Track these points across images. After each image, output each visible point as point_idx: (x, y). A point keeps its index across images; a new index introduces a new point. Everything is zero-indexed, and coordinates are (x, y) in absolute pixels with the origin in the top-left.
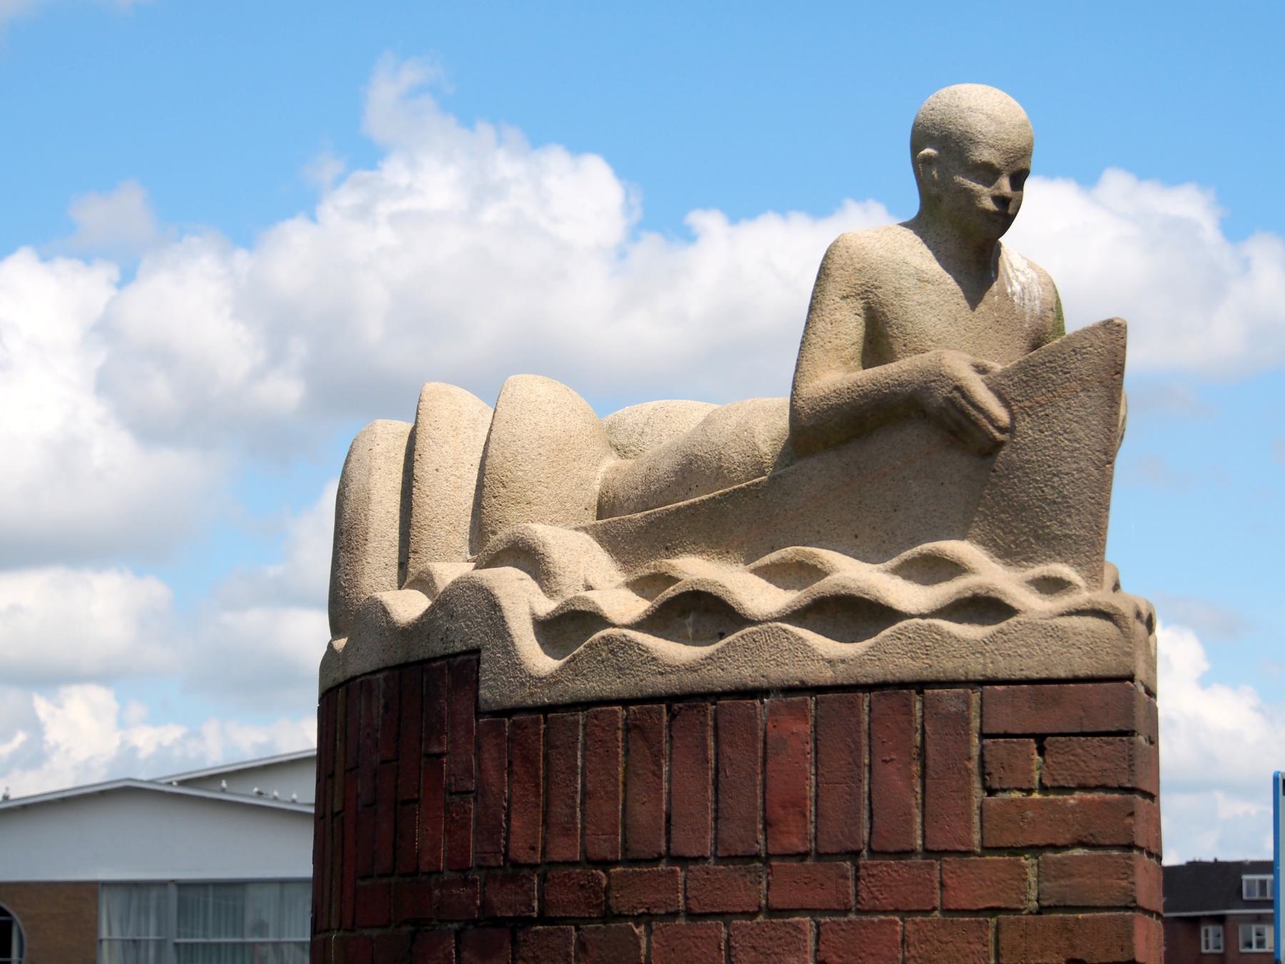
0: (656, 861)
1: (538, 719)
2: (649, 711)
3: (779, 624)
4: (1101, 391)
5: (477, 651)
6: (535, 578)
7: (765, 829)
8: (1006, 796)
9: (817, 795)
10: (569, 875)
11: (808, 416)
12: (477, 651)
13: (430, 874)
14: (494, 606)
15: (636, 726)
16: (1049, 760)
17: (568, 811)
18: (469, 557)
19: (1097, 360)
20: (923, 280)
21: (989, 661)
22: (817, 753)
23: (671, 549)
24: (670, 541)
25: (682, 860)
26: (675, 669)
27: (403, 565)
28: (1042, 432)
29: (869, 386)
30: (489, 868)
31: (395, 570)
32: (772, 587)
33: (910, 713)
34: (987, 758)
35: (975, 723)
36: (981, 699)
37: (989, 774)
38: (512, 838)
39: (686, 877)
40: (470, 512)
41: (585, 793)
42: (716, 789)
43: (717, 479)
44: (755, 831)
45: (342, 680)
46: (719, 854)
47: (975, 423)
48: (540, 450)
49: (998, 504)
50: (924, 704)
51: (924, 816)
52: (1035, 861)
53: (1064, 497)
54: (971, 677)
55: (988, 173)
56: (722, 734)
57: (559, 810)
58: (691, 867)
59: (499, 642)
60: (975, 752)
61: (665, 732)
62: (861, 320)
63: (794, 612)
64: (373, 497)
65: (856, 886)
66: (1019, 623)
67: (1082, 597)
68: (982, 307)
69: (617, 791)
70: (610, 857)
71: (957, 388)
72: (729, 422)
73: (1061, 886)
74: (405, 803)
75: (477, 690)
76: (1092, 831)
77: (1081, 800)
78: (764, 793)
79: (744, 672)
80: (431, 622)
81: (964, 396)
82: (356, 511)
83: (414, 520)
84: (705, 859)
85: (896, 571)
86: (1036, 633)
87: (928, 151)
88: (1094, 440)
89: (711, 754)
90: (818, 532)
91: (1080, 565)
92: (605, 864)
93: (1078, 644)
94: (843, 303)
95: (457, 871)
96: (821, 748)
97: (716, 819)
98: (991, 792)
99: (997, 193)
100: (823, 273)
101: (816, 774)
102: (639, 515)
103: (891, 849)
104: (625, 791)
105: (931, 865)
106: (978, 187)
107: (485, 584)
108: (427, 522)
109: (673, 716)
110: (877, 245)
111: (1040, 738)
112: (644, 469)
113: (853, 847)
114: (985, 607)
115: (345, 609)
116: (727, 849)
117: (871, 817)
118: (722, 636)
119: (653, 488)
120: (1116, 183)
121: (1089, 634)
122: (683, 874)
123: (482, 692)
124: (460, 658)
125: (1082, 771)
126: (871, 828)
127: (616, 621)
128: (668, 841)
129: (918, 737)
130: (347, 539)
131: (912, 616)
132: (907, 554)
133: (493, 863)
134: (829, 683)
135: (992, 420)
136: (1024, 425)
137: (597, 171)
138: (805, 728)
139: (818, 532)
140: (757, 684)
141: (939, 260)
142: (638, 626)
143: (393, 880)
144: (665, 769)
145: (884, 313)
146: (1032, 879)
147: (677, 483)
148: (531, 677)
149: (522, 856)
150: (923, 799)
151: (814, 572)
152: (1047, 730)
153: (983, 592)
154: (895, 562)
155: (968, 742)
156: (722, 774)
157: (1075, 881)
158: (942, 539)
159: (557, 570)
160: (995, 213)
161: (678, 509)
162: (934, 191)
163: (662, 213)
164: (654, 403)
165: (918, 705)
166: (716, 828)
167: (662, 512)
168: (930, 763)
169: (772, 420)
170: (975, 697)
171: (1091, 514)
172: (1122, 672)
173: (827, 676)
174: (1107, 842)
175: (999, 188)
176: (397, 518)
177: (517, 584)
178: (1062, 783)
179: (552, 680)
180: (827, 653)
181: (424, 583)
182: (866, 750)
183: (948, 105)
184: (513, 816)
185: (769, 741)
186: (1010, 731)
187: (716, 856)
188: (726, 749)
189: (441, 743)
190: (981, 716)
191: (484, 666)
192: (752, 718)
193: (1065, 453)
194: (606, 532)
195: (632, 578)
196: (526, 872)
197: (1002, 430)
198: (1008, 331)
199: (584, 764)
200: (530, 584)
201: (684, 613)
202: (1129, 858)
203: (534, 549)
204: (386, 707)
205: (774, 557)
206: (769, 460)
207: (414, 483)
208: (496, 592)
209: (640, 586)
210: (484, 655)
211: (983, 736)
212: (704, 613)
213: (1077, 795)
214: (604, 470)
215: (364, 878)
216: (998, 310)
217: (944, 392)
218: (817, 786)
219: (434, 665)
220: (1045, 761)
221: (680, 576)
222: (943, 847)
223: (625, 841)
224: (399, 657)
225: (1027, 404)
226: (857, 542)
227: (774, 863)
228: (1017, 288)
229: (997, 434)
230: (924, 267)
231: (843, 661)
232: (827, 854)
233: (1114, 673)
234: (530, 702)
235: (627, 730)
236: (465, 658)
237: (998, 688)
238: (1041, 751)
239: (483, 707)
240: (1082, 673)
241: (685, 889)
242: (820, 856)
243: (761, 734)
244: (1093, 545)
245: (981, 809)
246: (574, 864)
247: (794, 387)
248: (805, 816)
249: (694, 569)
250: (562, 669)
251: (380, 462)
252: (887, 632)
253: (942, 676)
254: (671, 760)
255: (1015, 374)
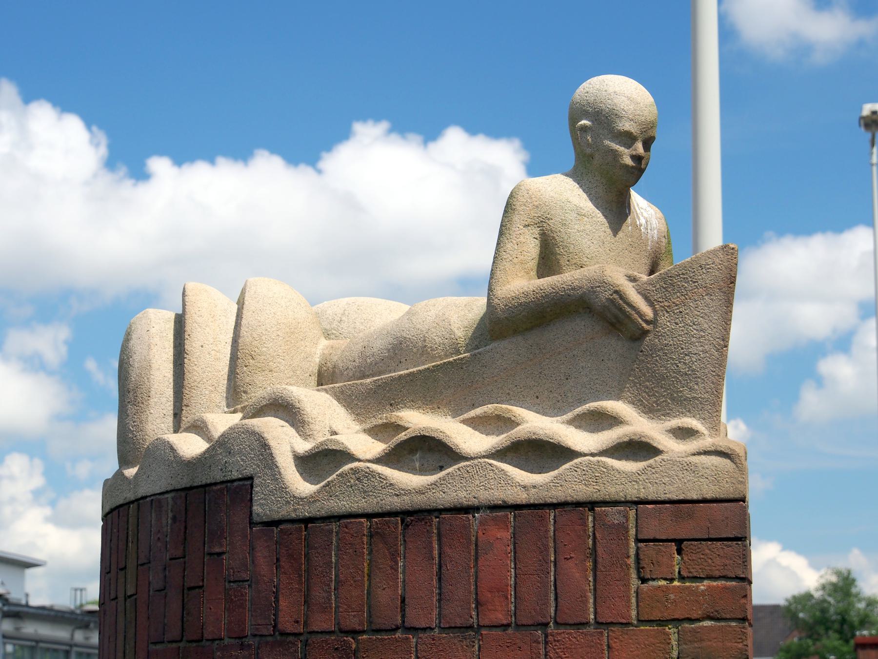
0: (395, 630)
1: (301, 528)
2: (387, 523)
3: (487, 460)
4: (719, 295)
5: (251, 478)
6: (292, 425)
7: (477, 607)
8: (655, 583)
9: (516, 583)
10: (326, 641)
11: (503, 311)
12: (251, 478)
13: (213, 640)
14: (265, 446)
15: (377, 533)
16: (685, 558)
17: (325, 595)
18: (226, 409)
19: (717, 273)
20: (580, 214)
21: (642, 487)
22: (515, 553)
23: (394, 405)
24: (394, 399)
25: (414, 630)
26: (408, 492)
27: (177, 415)
28: (677, 324)
29: (549, 290)
30: (261, 636)
31: (170, 419)
32: (477, 433)
33: (585, 524)
34: (641, 557)
35: (632, 532)
36: (637, 514)
37: (643, 568)
38: (281, 614)
39: (417, 642)
40: (226, 377)
41: (338, 582)
42: (440, 579)
43: (422, 355)
44: (469, 609)
45: (133, 498)
46: (442, 626)
47: (628, 317)
48: (279, 333)
49: (644, 375)
50: (594, 518)
51: (595, 598)
52: (676, 630)
53: (693, 370)
54: (629, 498)
55: (628, 139)
56: (444, 540)
57: (318, 594)
58: (420, 635)
59: (269, 472)
60: (632, 552)
61: (400, 537)
62: (537, 242)
63: (497, 451)
64: (153, 366)
65: (545, 648)
66: (663, 460)
67: (707, 441)
68: (621, 234)
69: (363, 580)
70: (358, 628)
71: (616, 292)
72: (429, 314)
73: (695, 648)
74: (190, 589)
75: (251, 506)
76: (717, 609)
77: (709, 587)
78: (476, 582)
79: (460, 495)
80: (212, 456)
81: (621, 298)
82: (140, 375)
83: (186, 382)
84: (432, 629)
85: (570, 422)
86: (675, 467)
87: (584, 122)
88: (715, 330)
89: (436, 553)
90: (509, 394)
91: (704, 419)
92: (354, 633)
93: (706, 475)
94: (525, 230)
95: (235, 638)
96: (518, 549)
97: (440, 601)
98: (644, 580)
99: (634, 153)
100: (509, 208)
101: (515, 568)
102: (368, 380)
103: (571, 622)
104: (369, 580)
105: (601, 633)
106: (621, 149)
107: (256, 429)
108: (196, 384)
109: (406, 526)
110: (549, 189)
111: (679, 542)
112: (359, 347)
113: (544, 621)
114: (637, 448)
115: (128, 446)
116: (449, 623)
117: (556, 599)
118: (441, 468)
119: (369, 361)
120: (454, 138)
121: (714, 468)
122: (415, 640)
123: (255, 508)
124: (236, 484)
125: (709, 565)
126: (556, 607)
127: (361, 457)
128: (403, 616)
129: (590, 542)
130: (129, 396)
131: (585, 455)
132: (579, 410)
133: (265, 632)
134: (524, 502)
135: (641, 315)
136: (663, 319)
137: (74, 125)
138: (506, 535)
139: (509, 394)
140: (470, 503)
141: (591, 200)
142: (378, 461)
143: (181, 645)
144: (401, 564)
145: (554, 238)
146: (674, 643)
147: (391, 358)
148: (294, 497)
149: (290, 628)
150: (595, 586)
151: (509, 423)
152: (684, 537)
153: (636, 438)
154: (570, 415)
155: (628, 545)
156: (444, 568)
157: (704, 644)
158: (602, 400)
159: (310, 420)
160: (632, 167)
161: (400, 376)
162: (588, 151)
163: (127, 158)
164: (347, 299)
165: (590, 519)
166: (440, 607)
167: (378, 379)
168: (600, 560)
169: (463, 313)
170: (632, 513)
171: (713, 383)
172: (737, 496)
173: (522, 497)
174: (728, 616)
175: (635, 150)
176: (171, 380)
177: (280, 429)
178: (695, 574)
179: (311, 500)
180: (522, 482)
181: (199, 428)
182: (552, 550)
183: (599, 90)
184: (281, 598)
185: (479, 544)
186: (658, 537)
187: (440, 627)
188: (448, 551)
189: (222, 546)
190: (637, 526)
191: (256, 489)
192: (466, 527)
193: (694, 340)
194: (342, 392)
195: (368, 426)
196: (291, 638)
197: (648, 322)
198: (638, 251)
199: (337, 561)
200: (290, 431)
201: (412, 451)
202: (744, 628)
203: (292, 405)
204: (174, 519)
205: (478, 411)
206: (462, 342)
207: (186, 356)
208: (266, 435)
209: (375, 432)
210: (257, 481)
211: (638, 540)
212: (429, 451)
213: (706, 582)
214: (319, 349)
215: (155, 643)
216: (631, 237)
217: (607, 294)
218: (516, 576)
219: (214, 488)
220: (682, 559)
221: (407, 425)
222: (609, 620)
223: (370, 615)
224: (185, 483)
225: (666, 304)
226: (538, 401)
227: (484, 632)
228: (643, 221)
229: (644, 325)
230: (582, 205)
231: (534, 487)
232: (524, 625)
233: (732, 496)
234: (293, 515)
235: (371, 536)
236: (241, 483)
237: (649, 506)
238: (679, 552)
239: (256, 519)
240: (709, 496)
241: (417, 651)
242: (518, 626)
243: (474, 539)
244: (714, 404)
245: (637, 593)
246: (332, 632)
247: (490, 290)
248: (507, 598)
249: (417, 420)
250: (318, 492)
251: (156, 340)
252: (567, 466)
253: (607, 498)
254: (404, 558)
255: (657, 282)
